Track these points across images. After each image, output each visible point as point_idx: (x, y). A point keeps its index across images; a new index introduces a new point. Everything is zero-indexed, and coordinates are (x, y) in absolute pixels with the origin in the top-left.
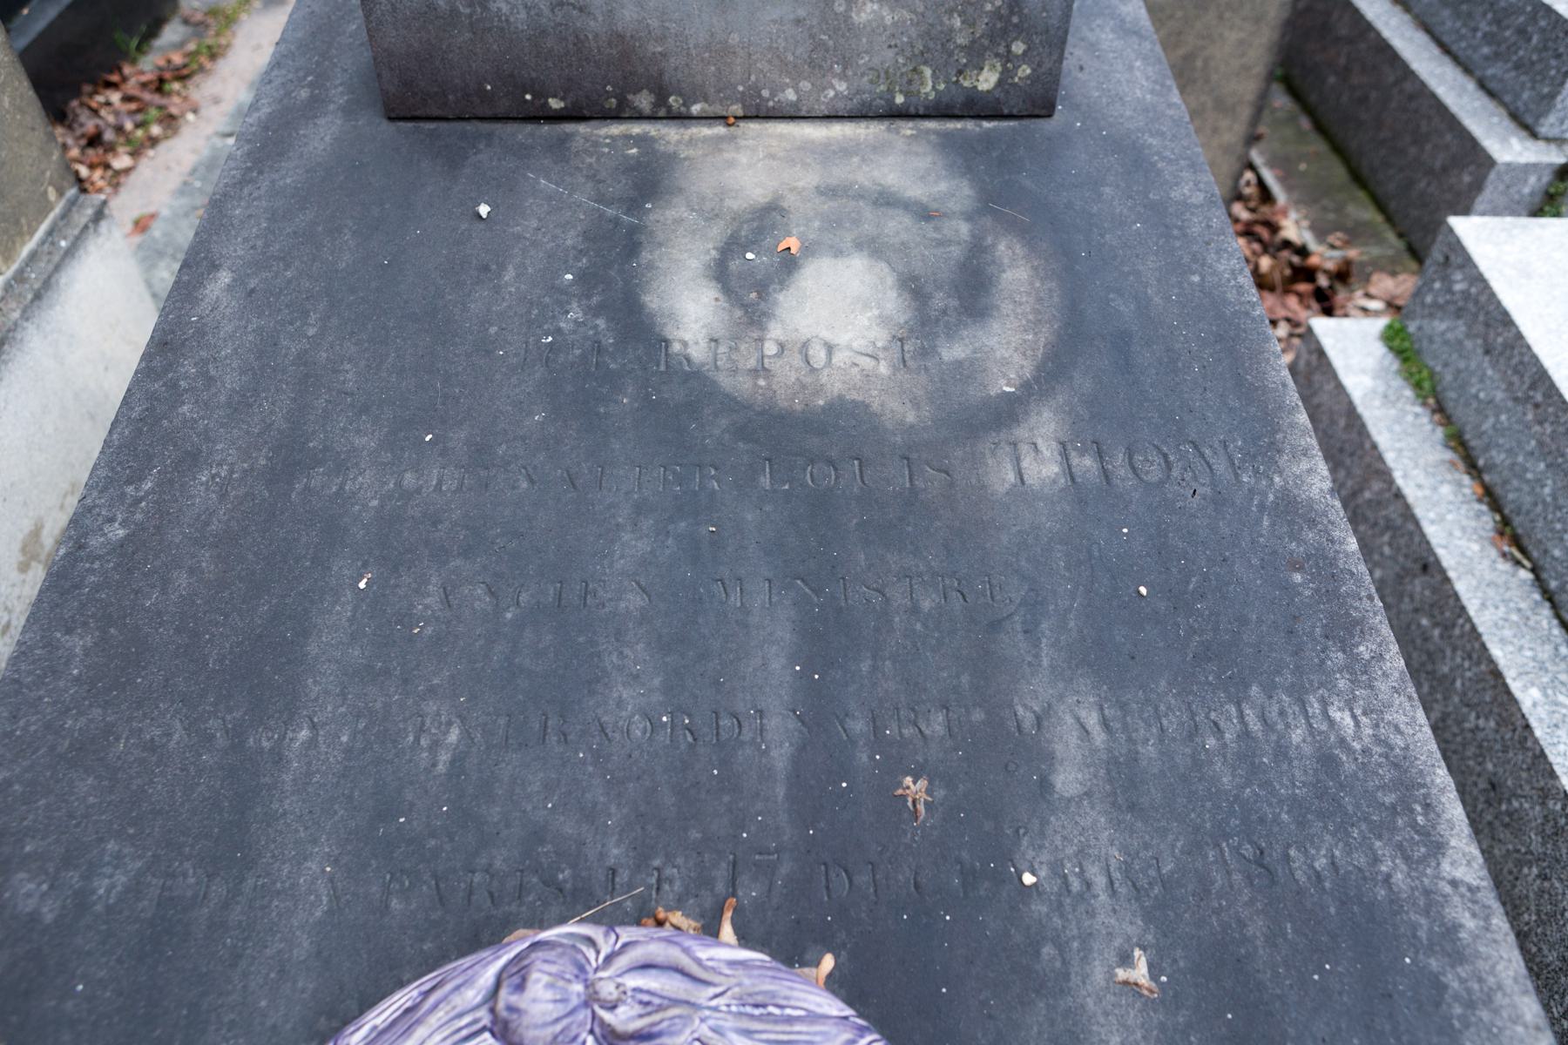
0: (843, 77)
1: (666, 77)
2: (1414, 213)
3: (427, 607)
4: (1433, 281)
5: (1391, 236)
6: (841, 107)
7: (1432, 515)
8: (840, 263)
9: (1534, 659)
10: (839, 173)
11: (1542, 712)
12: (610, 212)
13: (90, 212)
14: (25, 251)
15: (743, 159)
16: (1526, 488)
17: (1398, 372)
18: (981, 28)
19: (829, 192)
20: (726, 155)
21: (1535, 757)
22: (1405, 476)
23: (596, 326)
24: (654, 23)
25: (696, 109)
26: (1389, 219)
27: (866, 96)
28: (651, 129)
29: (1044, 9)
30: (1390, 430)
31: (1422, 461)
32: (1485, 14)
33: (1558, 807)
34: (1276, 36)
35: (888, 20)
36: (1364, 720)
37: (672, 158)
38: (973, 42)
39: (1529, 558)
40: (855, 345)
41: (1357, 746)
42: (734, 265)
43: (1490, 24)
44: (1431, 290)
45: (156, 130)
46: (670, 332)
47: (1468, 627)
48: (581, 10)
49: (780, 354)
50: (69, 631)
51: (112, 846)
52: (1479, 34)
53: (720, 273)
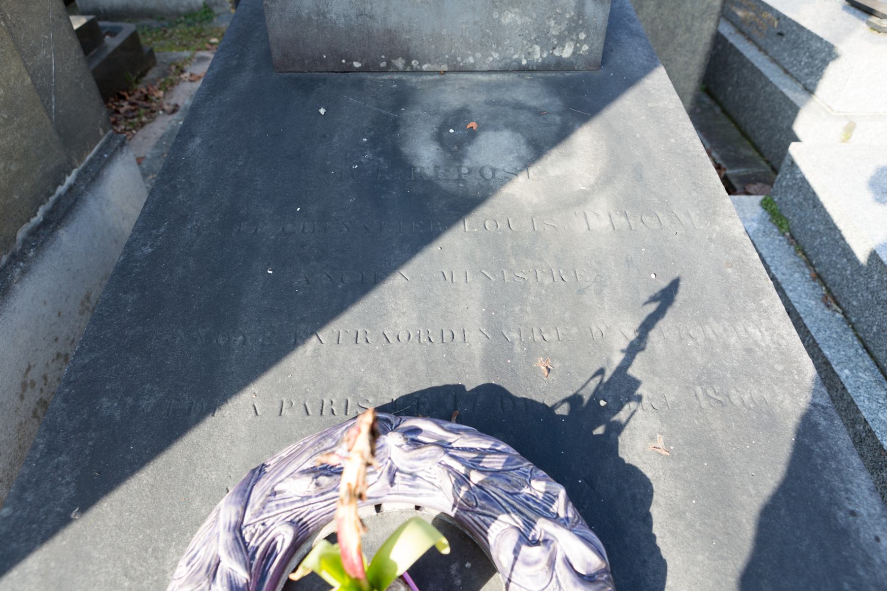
0: (496, 51)
1: (411, 51)
2: (774, 151)
3: (299, 283)
4: (786, 174)
5: (763, 163)
6: (496, 66)
7: (790, 288)
8: (498, 134)
9: (845, 355)
10: (495, 95)
11: (851, 381)
12: (384, 112)
13: (118, 141)
14: (88, 158)
15: (449, 89)
16: (837, 272)
17: (770, 220)
18: (563, 27)
19: (489, 103)
20: (440, 88)
21: (848, 403)
22: (776, 269)
23: (379, 161)
24: (406, 24)
25: (425, 67)
26: (761, 155)
27: (508, 60)
28: (404, 77)
29: (595, 17)
30: (767, 248)
31: (784, 263)
32: (805, 54)
33: (862, 428)
34: (703, 60)
35: (519, 22)
36: (766, 333)
37: (414, 89)
38: (561, 33)
39: (841, 308)
40: (506, 169)
41: (763, 344)
42: (445, 134)
43: (808, 58)
44: (785, 179)
45: (144, 119)
46: (415, 163)
47: (811, 341)
48: (371, 18)
49: (470, 172)
50: (125, 293)
51: (148, 386)
52: (803, 63)
53: (439, 138)
